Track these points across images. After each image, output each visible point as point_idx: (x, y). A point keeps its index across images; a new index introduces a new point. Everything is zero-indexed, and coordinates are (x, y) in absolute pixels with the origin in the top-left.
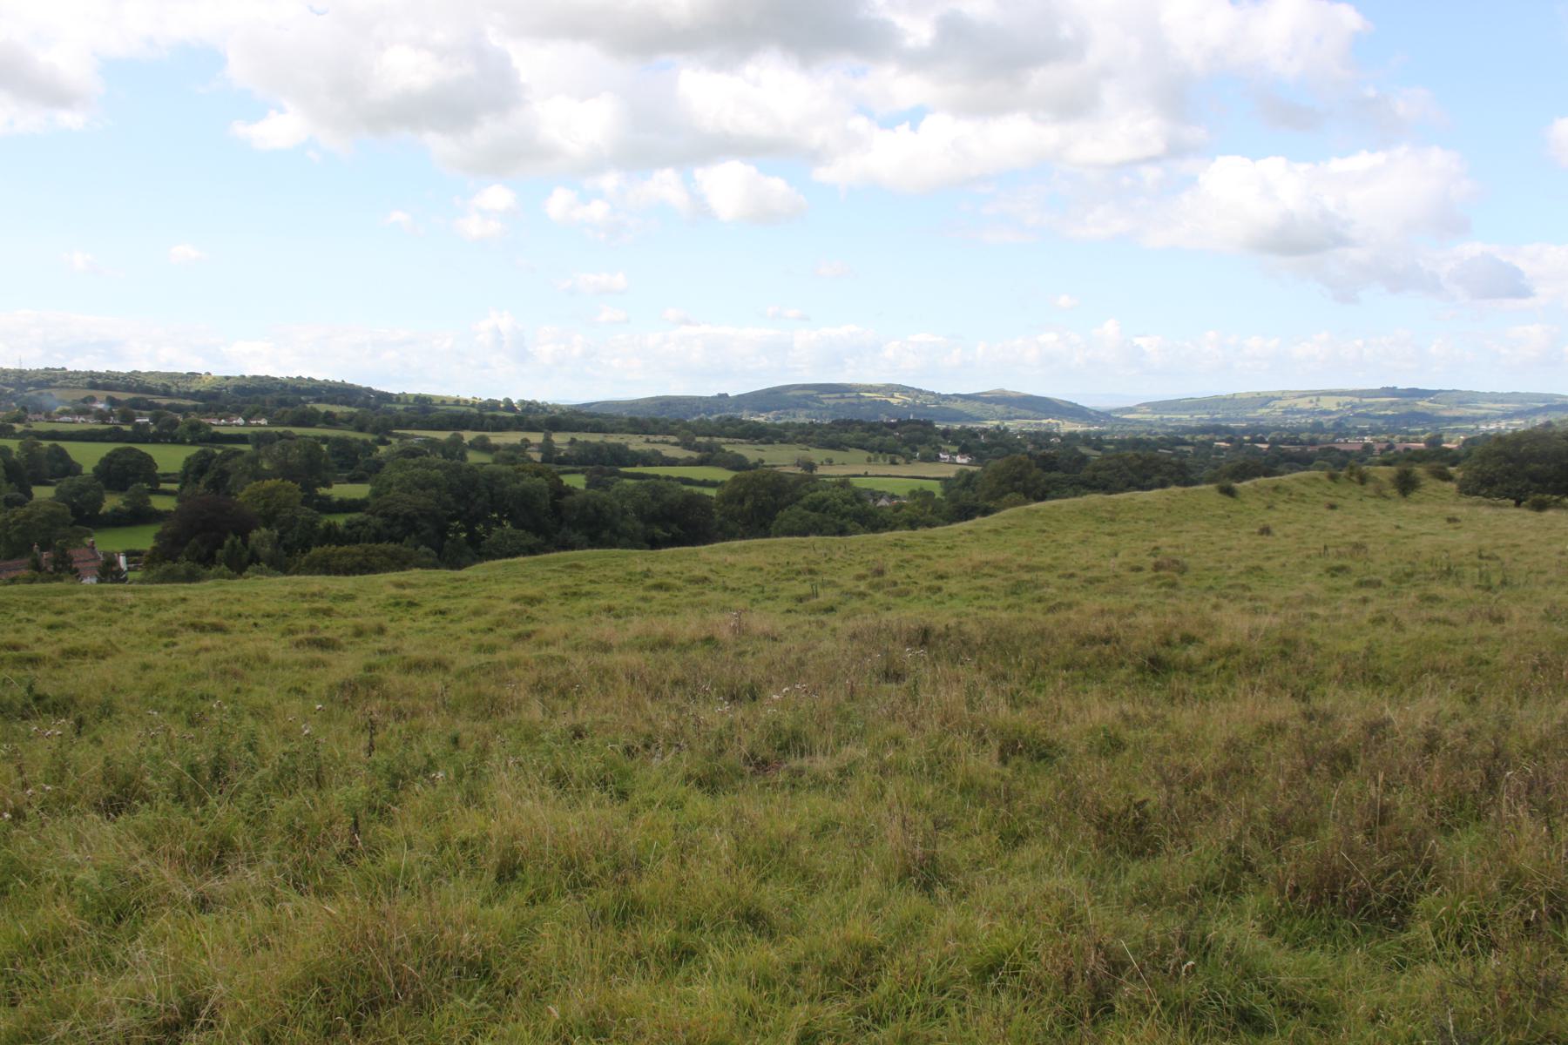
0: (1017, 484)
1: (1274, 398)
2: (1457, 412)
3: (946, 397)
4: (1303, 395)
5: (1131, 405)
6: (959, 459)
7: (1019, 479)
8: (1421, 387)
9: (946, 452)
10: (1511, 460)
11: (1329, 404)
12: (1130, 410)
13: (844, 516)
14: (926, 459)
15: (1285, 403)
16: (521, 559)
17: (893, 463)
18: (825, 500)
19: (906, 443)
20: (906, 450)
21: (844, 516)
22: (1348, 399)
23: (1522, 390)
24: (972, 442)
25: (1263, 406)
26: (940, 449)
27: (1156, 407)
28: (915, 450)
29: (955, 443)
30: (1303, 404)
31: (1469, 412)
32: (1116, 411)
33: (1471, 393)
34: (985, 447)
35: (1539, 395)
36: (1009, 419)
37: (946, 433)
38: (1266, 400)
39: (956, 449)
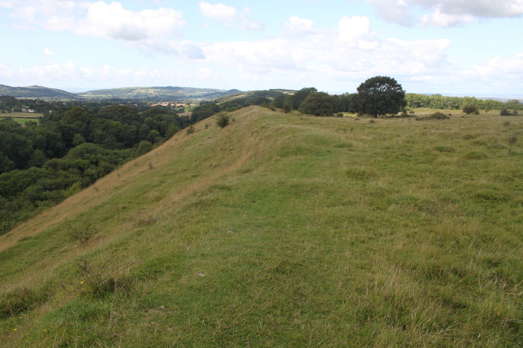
0: (80, 117)
1: (133, 89)
2: (190, 94)
3: (14, 88)
4: (143, 89)
5: (85, 91)
6: (30, 111)
7: (79, 116)
8: (179, 86)
9: (24, 108)
10: (318, 102)
11: (151, 91)
12: (85, 93)
13: (13, 132)
14: (16, 111)
15: (137, 91)
16: (243, 109)
17: (3, 112)
18: (3, 126)
19: (7, 104)
20: (8, 107)
21: (13, 132)
22: (157, 90)
23: (208, 88)
24: (34, 104)
25: (130, 92)
26: (21, 107)
27: (94, 92)
28: (12, 108)
29: (27, 105)
30: (143, 91)
31: (193, 94)
32: (80, 94)
33: (193, 88)
34: (40, 106)
35: (212, 89)
36: (41, 96)
37: (22, 101)
38: (131, 90)
39: (28, 107)
